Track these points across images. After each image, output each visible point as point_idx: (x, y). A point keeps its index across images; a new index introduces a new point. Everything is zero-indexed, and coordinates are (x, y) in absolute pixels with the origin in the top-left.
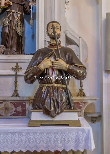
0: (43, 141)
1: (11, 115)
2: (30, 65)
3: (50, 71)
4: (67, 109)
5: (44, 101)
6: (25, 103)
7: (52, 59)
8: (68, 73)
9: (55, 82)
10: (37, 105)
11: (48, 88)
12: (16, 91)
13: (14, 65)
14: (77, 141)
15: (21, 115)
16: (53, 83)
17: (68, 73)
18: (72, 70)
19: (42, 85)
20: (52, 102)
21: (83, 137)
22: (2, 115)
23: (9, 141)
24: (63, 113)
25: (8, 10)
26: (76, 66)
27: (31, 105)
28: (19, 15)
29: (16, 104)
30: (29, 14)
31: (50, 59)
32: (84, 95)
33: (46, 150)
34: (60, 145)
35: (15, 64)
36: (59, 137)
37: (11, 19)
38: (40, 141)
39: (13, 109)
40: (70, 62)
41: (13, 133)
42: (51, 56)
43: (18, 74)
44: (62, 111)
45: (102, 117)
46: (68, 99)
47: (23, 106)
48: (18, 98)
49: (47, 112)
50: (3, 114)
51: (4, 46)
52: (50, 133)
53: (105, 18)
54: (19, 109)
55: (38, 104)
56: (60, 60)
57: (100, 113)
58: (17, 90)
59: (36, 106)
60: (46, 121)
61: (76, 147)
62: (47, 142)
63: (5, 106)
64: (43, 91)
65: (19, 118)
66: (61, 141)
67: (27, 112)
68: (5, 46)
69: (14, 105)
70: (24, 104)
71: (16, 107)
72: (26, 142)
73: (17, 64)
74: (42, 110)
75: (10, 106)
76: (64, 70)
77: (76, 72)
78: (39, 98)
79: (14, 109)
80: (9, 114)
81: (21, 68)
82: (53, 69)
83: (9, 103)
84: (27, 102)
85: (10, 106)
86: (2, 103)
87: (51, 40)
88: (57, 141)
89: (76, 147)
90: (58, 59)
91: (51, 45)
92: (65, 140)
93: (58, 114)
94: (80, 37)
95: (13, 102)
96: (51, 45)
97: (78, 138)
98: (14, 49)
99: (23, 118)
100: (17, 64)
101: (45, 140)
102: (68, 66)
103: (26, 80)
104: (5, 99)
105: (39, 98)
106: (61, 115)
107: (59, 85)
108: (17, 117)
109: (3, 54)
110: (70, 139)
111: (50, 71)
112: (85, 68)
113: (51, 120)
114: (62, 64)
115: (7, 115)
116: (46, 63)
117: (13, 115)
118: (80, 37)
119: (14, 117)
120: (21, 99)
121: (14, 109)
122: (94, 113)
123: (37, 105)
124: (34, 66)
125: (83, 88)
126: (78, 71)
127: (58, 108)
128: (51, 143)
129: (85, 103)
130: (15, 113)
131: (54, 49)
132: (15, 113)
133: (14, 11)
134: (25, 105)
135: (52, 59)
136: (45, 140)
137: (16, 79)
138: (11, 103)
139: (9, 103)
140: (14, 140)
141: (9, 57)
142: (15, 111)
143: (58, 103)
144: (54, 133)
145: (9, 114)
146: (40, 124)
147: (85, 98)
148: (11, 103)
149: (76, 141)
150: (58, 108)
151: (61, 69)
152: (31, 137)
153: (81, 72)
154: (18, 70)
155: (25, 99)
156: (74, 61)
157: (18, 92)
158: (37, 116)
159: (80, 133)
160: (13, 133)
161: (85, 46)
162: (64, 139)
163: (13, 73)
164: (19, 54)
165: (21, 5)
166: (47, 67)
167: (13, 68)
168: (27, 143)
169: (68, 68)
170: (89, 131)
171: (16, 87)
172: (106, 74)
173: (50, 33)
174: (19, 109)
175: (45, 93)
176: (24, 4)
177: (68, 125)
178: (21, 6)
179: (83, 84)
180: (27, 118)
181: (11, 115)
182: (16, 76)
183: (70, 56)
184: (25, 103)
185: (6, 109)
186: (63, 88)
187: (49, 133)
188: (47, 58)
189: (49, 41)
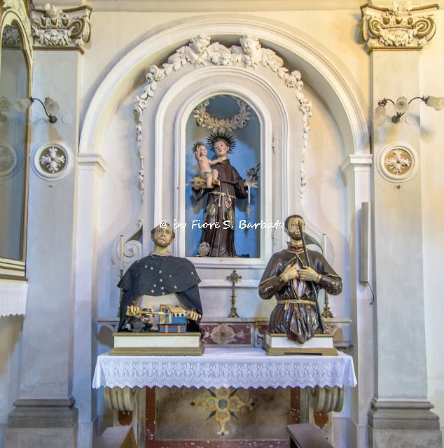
0: (289, 374)
1: (229, 343)
2: (267, 275)
3: (295, 282)
4: (317, 333)
5: (289, 323)
6: (249, 326)
7: (297, 266)
8: (322, 285)
9: (302, 298)
10: (278, 328)
11: (292, 306)
12: (234, 309)
13: (230, 273)
14: (334, 374)
15: (244, 343)
16: (298, 299)
17: (322, 285)
18: (325, 281)
19: (282, 302)
20: (299, 323)
21: (342, 369)
22: (216, 343)
23: (245, 373)
24: (313, 339)
25: (215, 192)
26: (330, 276)
27: (257, 329)
28: (230, 200)
29: (237, 327)
30: (245, 197)
31: (293, 267)
32: (331, 316)
33: (188, 386)
34: (311, 379)
35: (231, 271)
36: (310, 369)
37: (219, 205)
38: (286, 374)
39: (231, 334)
40: (321, 270)
41: (250, 364)
42: (295, 263)
43: (236, 285)
44: (312, 336)
45: (355, 347)
46: (319, 320)
47: (247, 331)
48: (235, 319)
49: (293, 337)
50: (218, 341)
51: (209, 245)
52: (298, 364)
53: (360, 207)
54: (241, 335)
55: (279, 327)
56: (310, 268)
57: (349, 342)
58: (235, 309)
59: (276, 330)
60: (291, 349)
61: (333, 382)
62: (295, 375)
63: (220, 330)
64: (285, 309)
65: (240, 347)
66: (313, 375)
67: (252, 339)
68: (210, 244)
69: (234, 329)
70: (248, 327)
71: (235, 332)
72: (266, 376)
73: (234, 271)
74: (286, 335)
75: (228, 330)
76: (314, 282)
77: (331, 284)
78: (280, 319)
79: (234, 335)
80: (227, 342)
81: (240, 277)
82: (298, 280)
83: (226, 326)
84: (251, 324)
85: (228, 330)
86: (217, 326)
87: (293, 240)
88: (308, 374)
89: (332, 382)
90: (307, 267)
91: (291, 247)
92: (318, 373)
93: (308, 339)
94: (324, 235)
95: (232, 324)
96: (291, 247)
97: (335, 371)
98: (223, 249)
99: (246, 347)
100: (234, 271)
101: (292, 373)
102: (320, 277)
103: (261, 294)
104: (221, 320)
105: (280, 319)
106: (310, 340)
107: (306, 302)
108: (237, 345)
109: (207, 256)
110: (325, 372)
111: (295, 282)
112: (340, 279)
113: (298, 347)
114: (312, 273)
115: (223, 343)
116: (291, 272)
117: (233, 343)
118: (324, 235)
119: (233, 345)
120: (244, 321)
121: (234, 335)
122: (342, 342)
123: (278, 328)
124: (273, 275)
125: (329, 306)
126: (333, 283)
127: (308, 331)
128: (300, 377)
129: (332, 327)
130: (235, 340)
131: (297, 254)
132: (235, 340)
133: (223, 194)
134: (250, 329)
135: (297, 266)
136: (292, 373)
137: (233, 292)
138: (229, 326)
139: (226, 326)
140: (252, 372)
141: (221, 261)
142: (236, 337)
143: (306, 324)
144: (304, 364)
145: (227, 342)
146: (283, 352)
147: (334, 320)
148: (229, 326)
149: (332, 374)
150: (308, 331)
151: (311, 280)
152: (273, 369)
153: (337, 285)
154: (237, 280)
155: (249, 321)
156: (326, 271)
157: (237, 311)
158: (278, 342)
159: (338, 364)
160: (250, 363)
161: (330, 245)
162: (317, 371)
163: (229, 284)
164: (230, 256)
165: (232, 184)
166: (292, 277)
167: (228, 278)
168: (269, 376)
169: (321, 279)
170: (349, 361)
171: (233, 304)
172: (361, 287)
173: (292, 232)
174: (241, 335)
175: (289, 311)
176: (237, 184)
177: (320, 354)
178: (232, 186)
179: (329, 300)
180: (252, 347)
181: (229, 343)
182: (233, 288)
183: (321, 264)
184: (249, 326)
185: (223, 334)
186: (312, 306)
187: (297, 364)
188: (290, 265)
189: (289, 241)
